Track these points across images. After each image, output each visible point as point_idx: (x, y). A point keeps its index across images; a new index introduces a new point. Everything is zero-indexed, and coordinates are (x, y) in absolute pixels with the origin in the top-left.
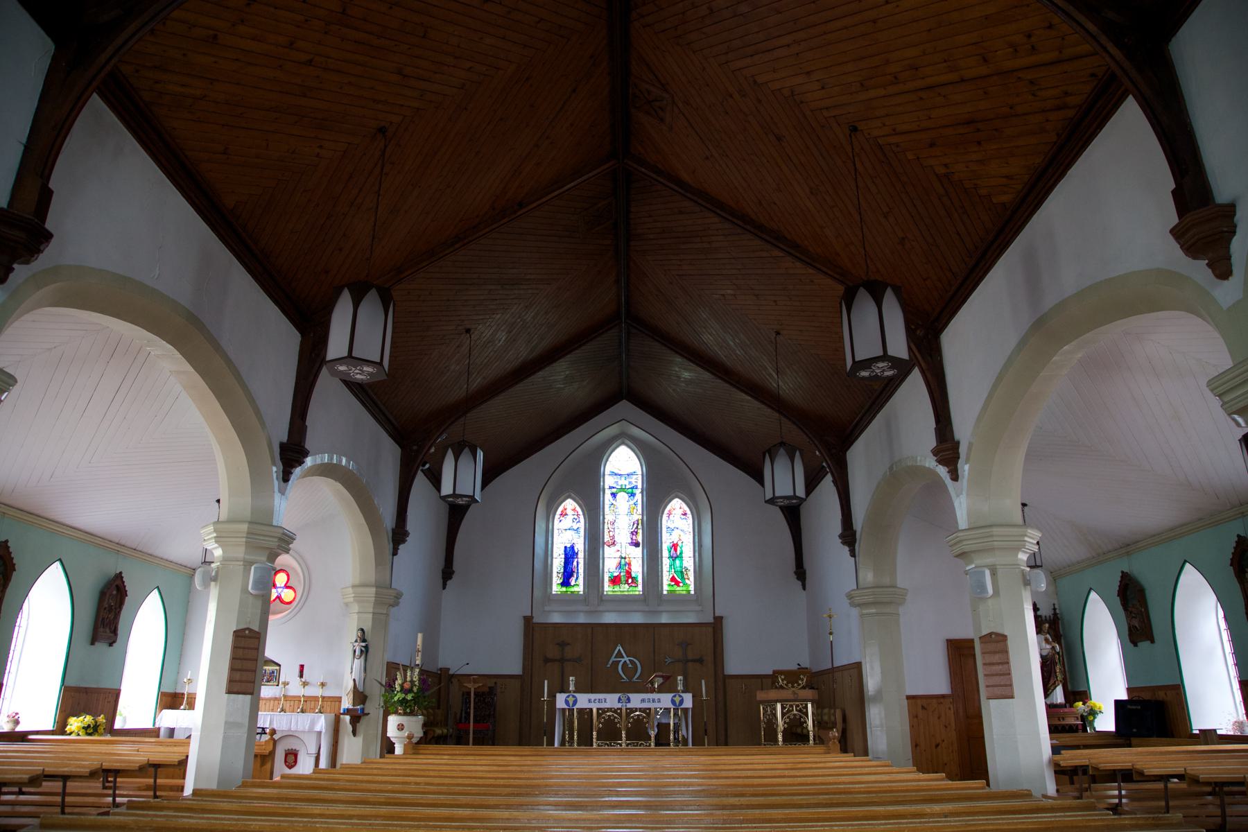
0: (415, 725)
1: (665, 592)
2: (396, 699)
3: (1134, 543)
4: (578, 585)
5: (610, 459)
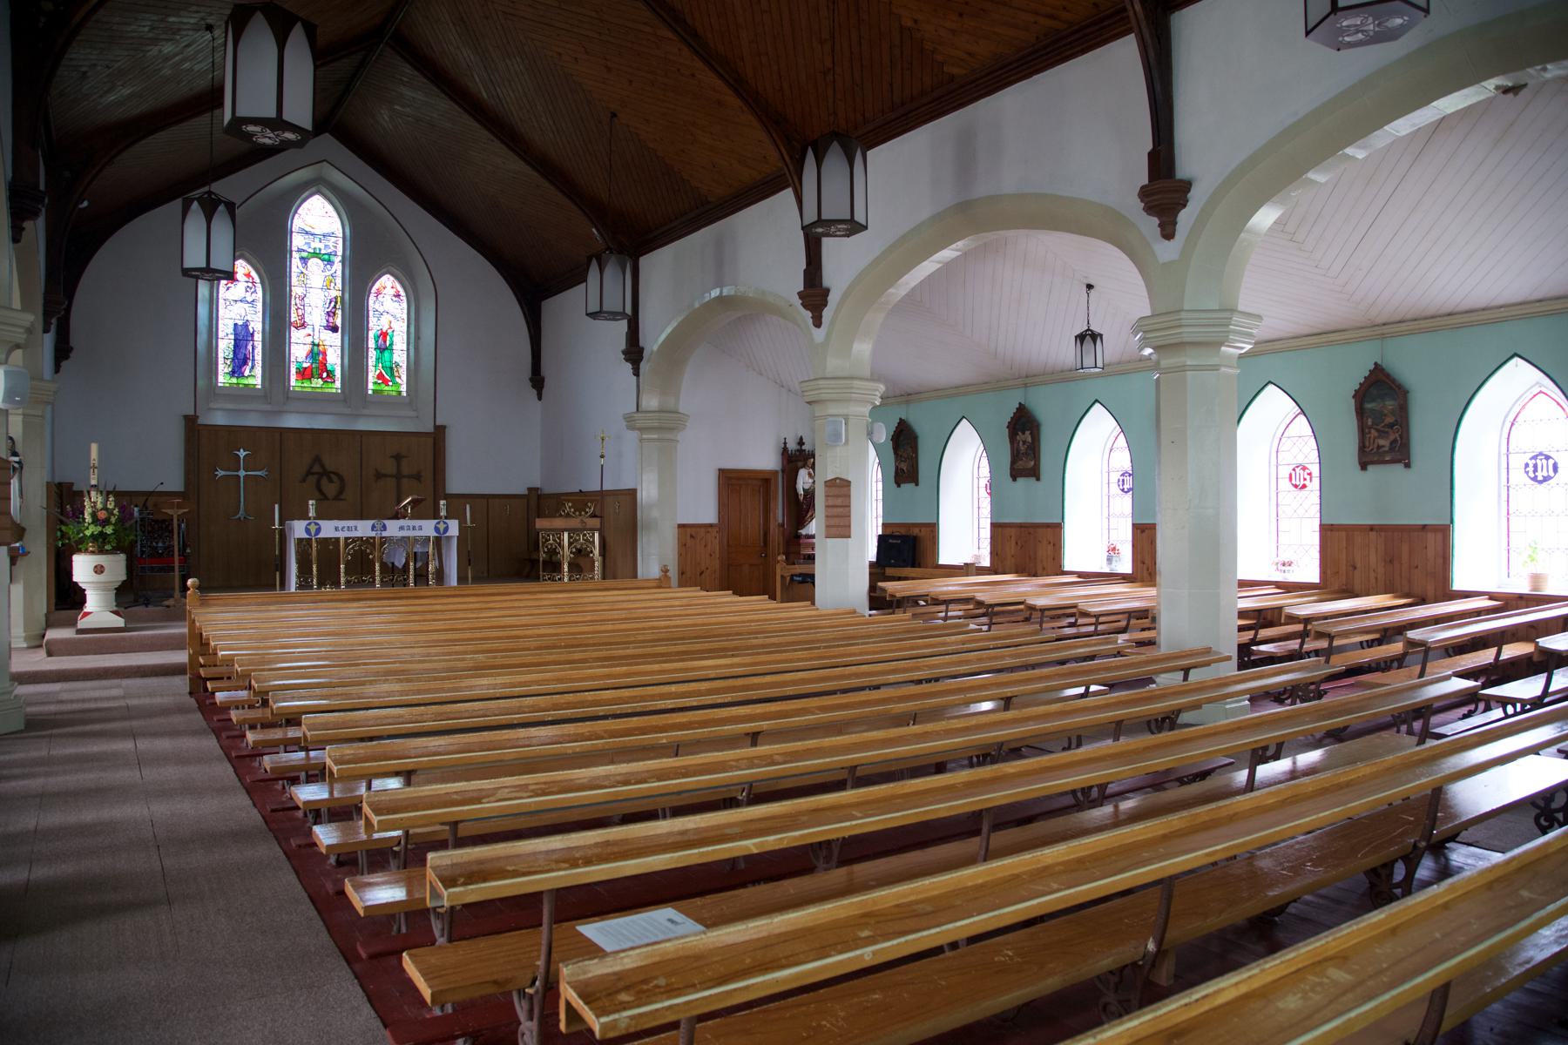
0: (116, 566)
1: (370, 392)
2: (88, 533)
3: (917, 393)
4: (254, 376)
5: (300, 211)
